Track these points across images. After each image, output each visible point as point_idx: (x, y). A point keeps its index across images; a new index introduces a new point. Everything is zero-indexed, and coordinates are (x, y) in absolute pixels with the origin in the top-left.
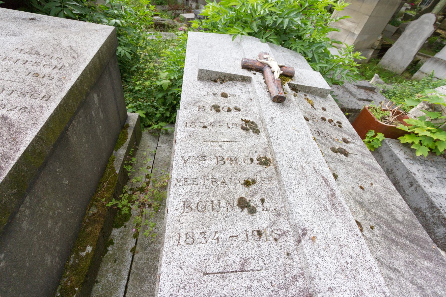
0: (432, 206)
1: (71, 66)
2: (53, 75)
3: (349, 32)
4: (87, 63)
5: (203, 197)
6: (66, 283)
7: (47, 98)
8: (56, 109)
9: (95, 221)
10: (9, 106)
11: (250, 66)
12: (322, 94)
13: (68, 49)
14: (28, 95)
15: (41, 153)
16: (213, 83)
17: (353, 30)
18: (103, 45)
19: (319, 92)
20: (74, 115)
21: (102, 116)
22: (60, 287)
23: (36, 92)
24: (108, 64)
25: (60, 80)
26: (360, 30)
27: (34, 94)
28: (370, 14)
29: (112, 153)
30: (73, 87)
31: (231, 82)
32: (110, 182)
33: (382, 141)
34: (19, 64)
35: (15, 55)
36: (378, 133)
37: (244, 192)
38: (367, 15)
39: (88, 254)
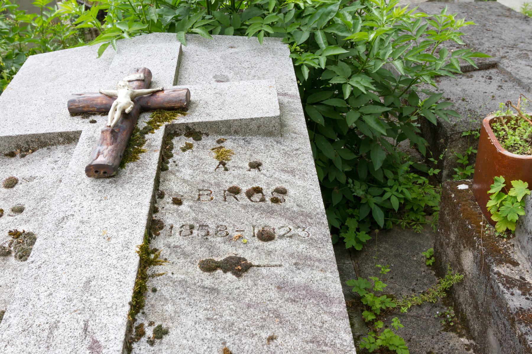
11: (83, 107)
16: (7, 159)
31: (45, 149)
36: (513, 183)
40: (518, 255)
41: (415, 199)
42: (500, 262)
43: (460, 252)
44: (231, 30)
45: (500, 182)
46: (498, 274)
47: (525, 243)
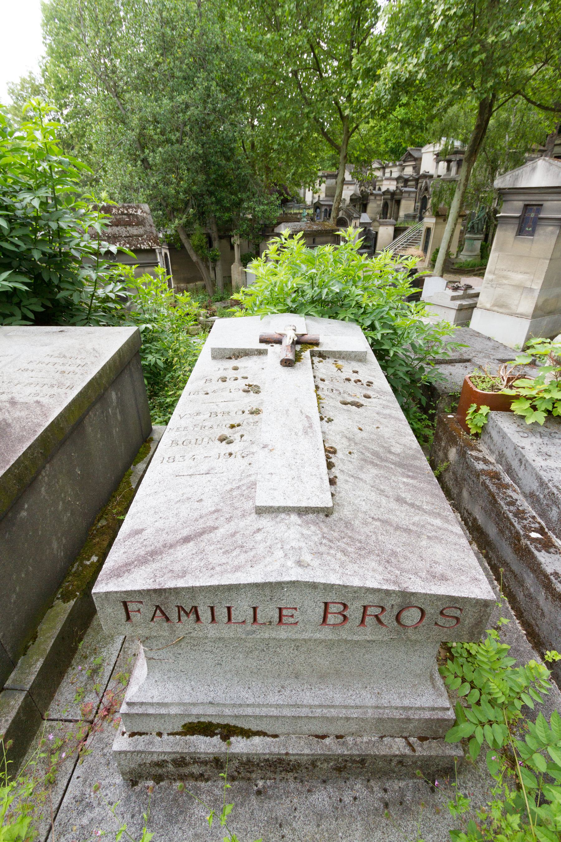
0: (542, 484)
1: (92, 363)
2: (76, 371)
3: (525, 289)
4: (107, 359)
5: (190, 437)
6: (68, 587)
7: (71, 388)
8: (78, 395)
9: (103, 533)
10: (41, 395)
12: (358, 358)
13: (92, 351)
14: (56, 387)
15: (62, 429)
17: (528, 284)
18: (124, 344)
19: (353, 355)
20: (93, 404)
21: (119, 417)
22: (61, 590)
23: (62, 384)
24: (129, 363)
25: (82, 374)
26: (540, 282)
27: (60, 385)
28: (549, 256)
29: (129, 467)
30: (93, 379)
32: (124, 496)
33: (487, 415)
34: (50, 366)
35: (47, 360)
36: (481, 407)
37: (227, 432)
38: (545, 258)
39: (92, 563)
40: (482, 447)
41: (419, 428)
42: (472, 450)
43: (448, 451)
44: (327, 316)
45: (474, 406)
46: (471, 455)
47: (486, 440)
